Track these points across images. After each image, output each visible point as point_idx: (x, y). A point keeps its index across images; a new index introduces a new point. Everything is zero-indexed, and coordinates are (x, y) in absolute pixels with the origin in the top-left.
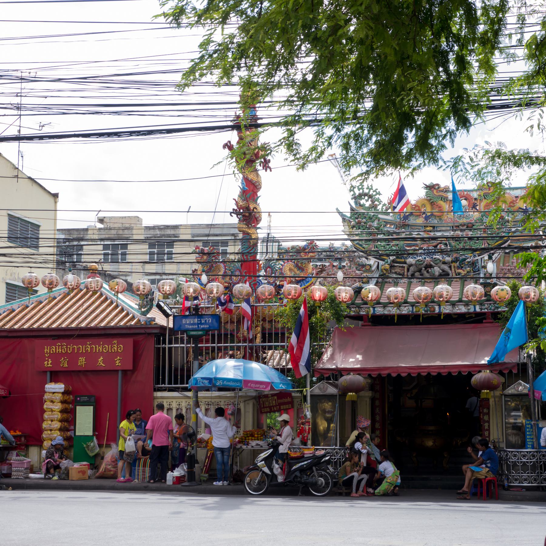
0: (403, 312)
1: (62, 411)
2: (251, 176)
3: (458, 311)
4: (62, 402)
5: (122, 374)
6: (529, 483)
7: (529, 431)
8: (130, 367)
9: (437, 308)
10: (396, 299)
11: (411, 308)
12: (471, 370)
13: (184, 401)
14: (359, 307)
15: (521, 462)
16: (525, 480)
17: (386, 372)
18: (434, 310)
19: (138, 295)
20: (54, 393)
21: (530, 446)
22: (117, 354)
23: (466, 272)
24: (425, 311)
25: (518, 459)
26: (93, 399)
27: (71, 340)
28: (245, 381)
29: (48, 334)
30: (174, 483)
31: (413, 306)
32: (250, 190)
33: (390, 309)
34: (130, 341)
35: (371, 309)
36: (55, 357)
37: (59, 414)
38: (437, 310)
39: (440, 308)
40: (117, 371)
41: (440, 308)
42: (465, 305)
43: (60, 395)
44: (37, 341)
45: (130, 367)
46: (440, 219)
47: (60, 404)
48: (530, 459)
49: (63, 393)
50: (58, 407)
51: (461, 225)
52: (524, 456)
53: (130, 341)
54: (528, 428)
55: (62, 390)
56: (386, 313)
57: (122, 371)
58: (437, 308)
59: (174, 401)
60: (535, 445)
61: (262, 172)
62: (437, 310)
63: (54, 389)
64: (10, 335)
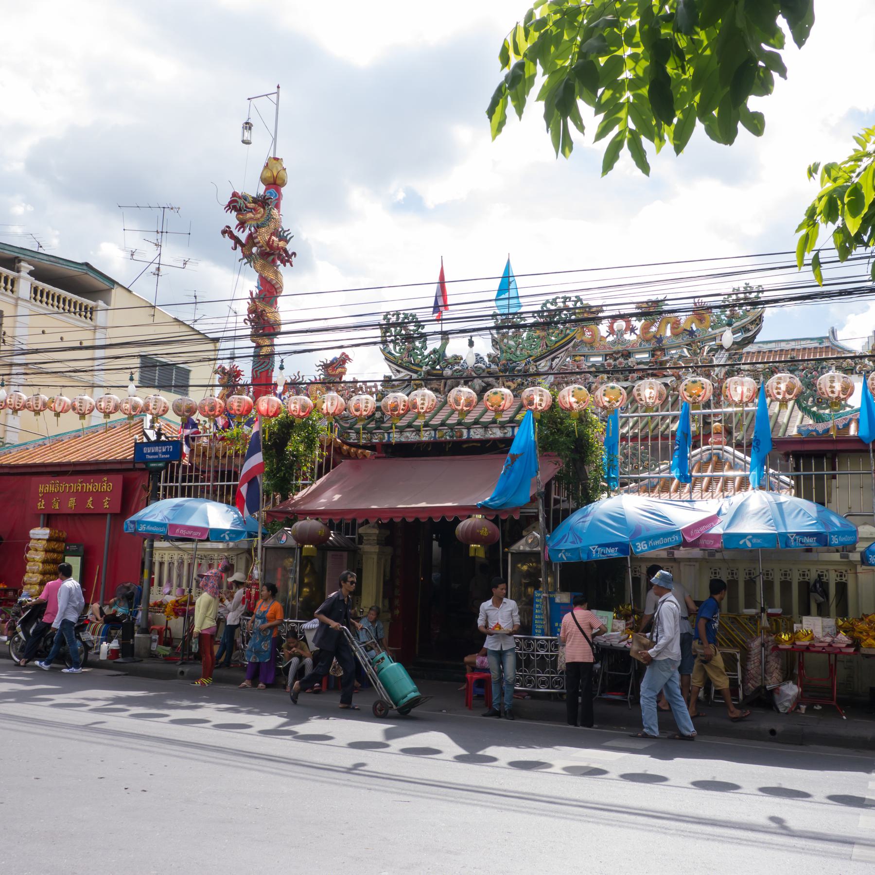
0: (424, 439)
1: (44, 562)
2: (271, 276)
3: (492, 436)
4: (46, 551)
5: (111, 518)
6: (548, 688)
7: (539, 608)
8: (118, 511)
9: (465, 432)
10: (357, 410)
11: (433, 432)
12: (458, 514)
13: (176, 552)
14: (372, 433)
15: (538, 655)
16: (543, 683)
17: (350, 516)
18: (461, 435)
19: (79, 413)
20: (39, 539)
21: (540, 632)
22: (105, 493)
23: (516, 385)
24: (450, 437)
25: (533, 651)
26: (81, 549)
27: (66, 478)
28: (171, 525)
29: (44, 470)
30: (109, 658)
31: (435, 430)
32: (269, 292)
33: (408, 434)
34: (120, 478)
35: (386, 435)
36: (48, 496)
37: (41, 565)
38: (465, 436)
39: (469, 432)
40: (106, 514)
41: (469, 432)
42: (500, 428)
43: (44, 542)
44: (35, 479)
45: (118, 511)
46: (592, 347)
47: (43, 553)
48: (551, 651)
49: (48, 540)
50: (40, 556)
51: (615, 352)
52: (542, 646)
53: (120, 478)
54: (538, 603)
55: (47, 537)
56: (403, 440)
57: (111, 514)
58: (465, 432)
59: (167, 552)
60: (546, 630)
61: (281, 268)
62: (465, 436)
63: (40, 533)
64: (12, 471)
